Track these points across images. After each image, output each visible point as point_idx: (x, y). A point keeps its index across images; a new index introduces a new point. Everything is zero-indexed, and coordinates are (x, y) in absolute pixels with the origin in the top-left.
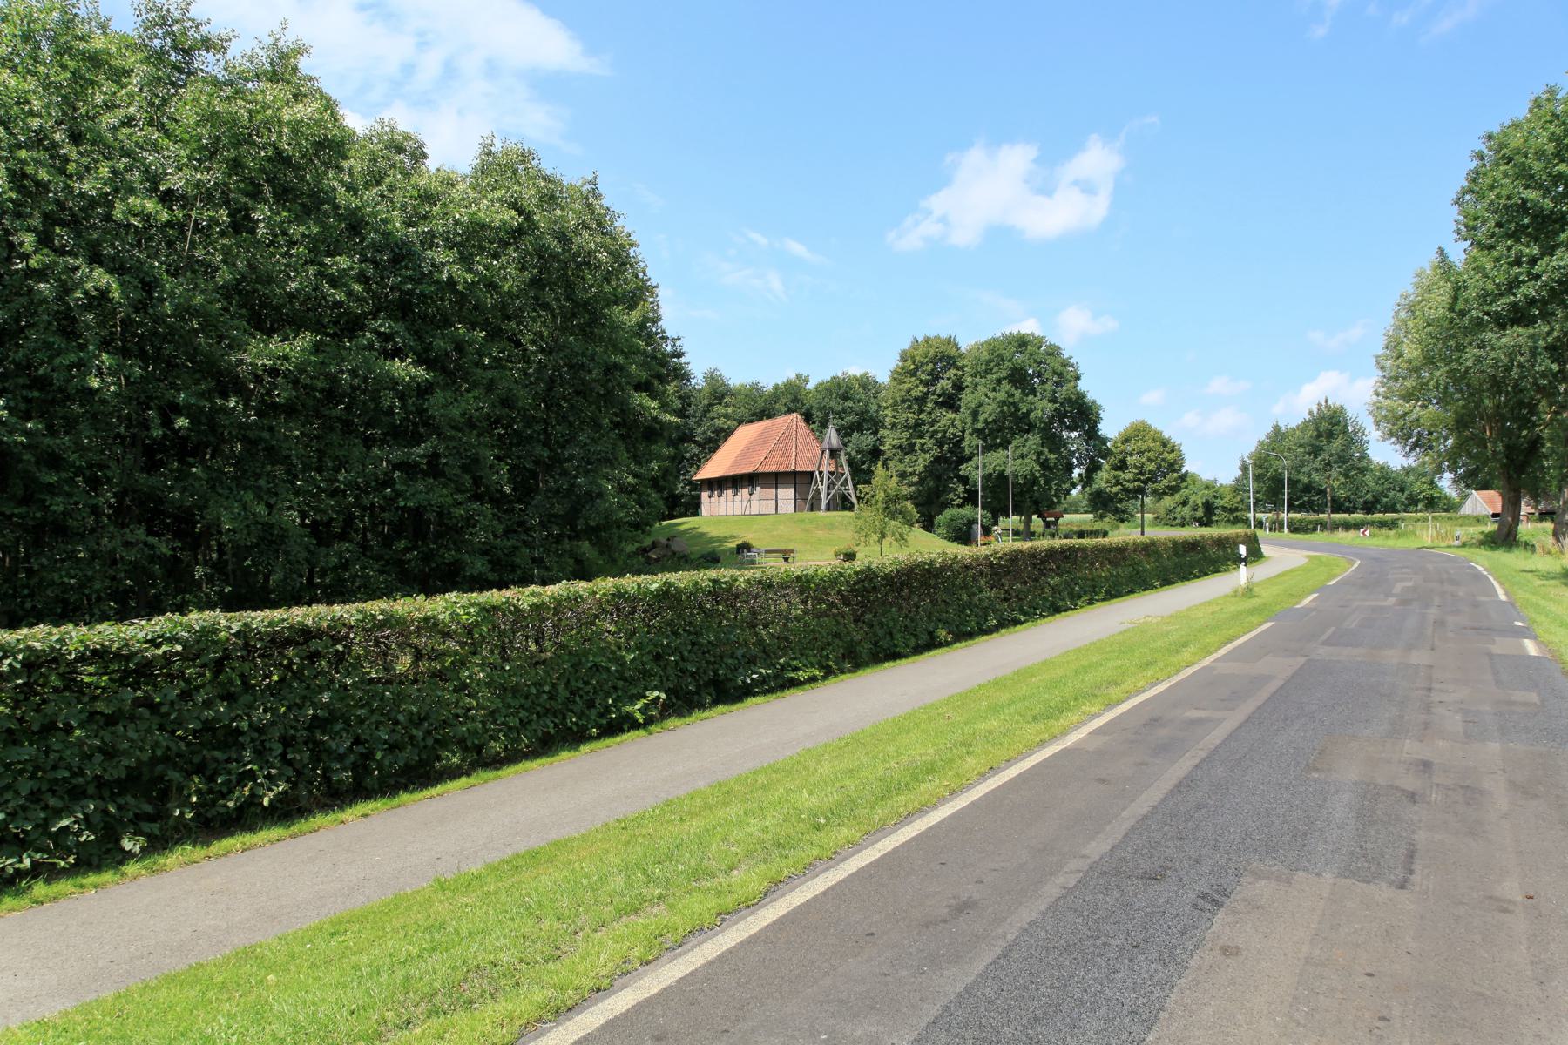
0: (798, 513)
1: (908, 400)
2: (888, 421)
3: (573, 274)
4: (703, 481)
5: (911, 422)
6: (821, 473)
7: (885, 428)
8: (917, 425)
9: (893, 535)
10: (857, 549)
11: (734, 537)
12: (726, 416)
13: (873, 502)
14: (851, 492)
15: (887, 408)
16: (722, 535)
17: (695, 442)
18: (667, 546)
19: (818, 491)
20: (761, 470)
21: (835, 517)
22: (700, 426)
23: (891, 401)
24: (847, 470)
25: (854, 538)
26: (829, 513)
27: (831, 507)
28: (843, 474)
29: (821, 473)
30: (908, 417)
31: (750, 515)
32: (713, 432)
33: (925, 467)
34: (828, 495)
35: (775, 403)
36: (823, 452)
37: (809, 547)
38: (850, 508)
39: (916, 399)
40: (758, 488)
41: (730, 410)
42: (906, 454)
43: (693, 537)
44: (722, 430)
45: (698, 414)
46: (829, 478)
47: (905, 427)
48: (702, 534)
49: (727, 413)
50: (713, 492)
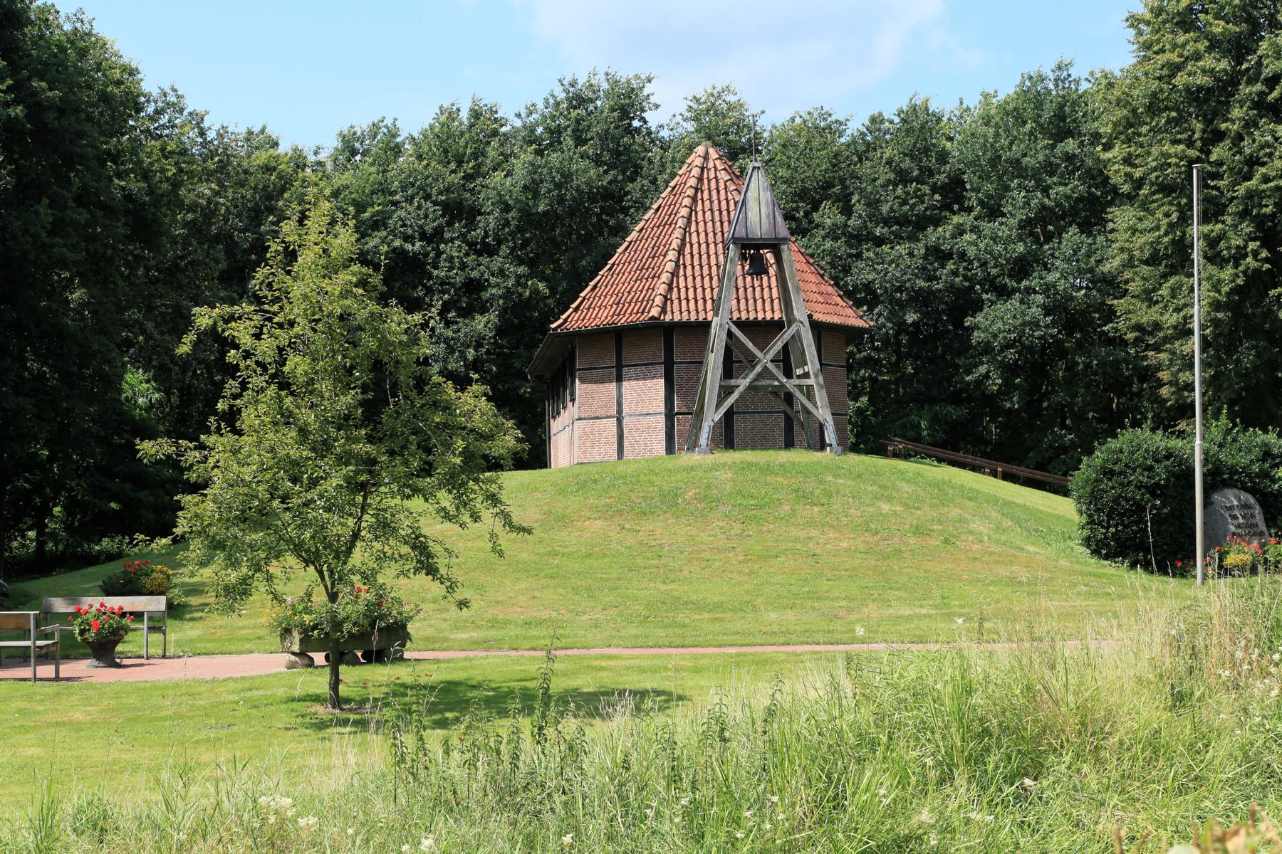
21: (715, 467)
30: (1165, 155)
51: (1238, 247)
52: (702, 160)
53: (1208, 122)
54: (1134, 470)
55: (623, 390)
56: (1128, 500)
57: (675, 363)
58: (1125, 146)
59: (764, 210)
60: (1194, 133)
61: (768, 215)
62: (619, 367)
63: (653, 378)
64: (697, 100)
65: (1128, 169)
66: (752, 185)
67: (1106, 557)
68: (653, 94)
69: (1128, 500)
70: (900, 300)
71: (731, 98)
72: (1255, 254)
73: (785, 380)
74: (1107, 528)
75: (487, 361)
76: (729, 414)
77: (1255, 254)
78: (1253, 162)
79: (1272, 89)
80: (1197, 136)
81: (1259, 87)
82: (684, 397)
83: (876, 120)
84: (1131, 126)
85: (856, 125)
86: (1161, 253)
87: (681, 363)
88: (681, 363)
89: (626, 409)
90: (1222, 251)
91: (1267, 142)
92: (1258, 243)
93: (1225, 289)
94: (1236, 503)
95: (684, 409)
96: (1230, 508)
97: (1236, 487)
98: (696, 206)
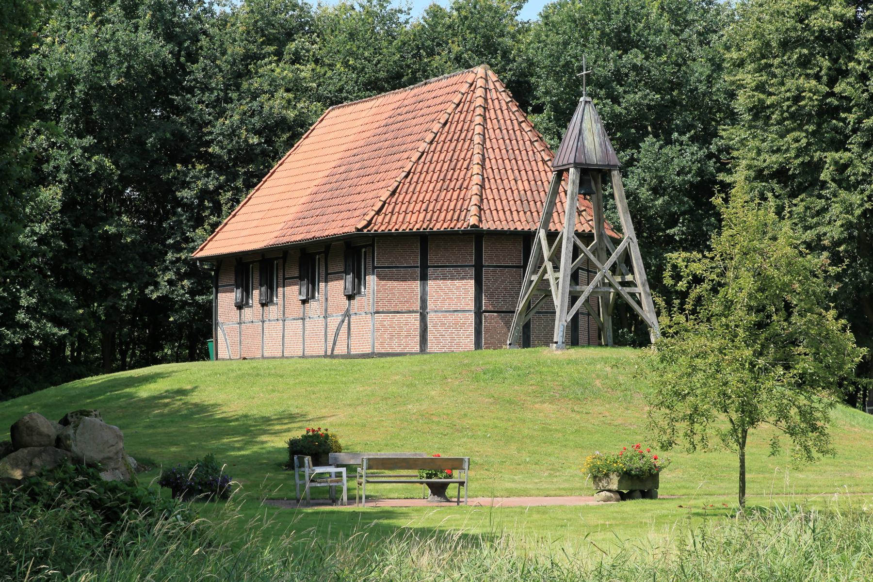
0: (484, 352)
1: (801, 42)
2: (741, 103)
3: (248, 97)
4: (221, 262)
5: (810, 103)
6: (552, 236)
7: (732, 117)
8: (826, 112)
9: (782, 414)
10: (663, 457)
11: (292, 418)
12: (296, 88)
13: (716, 307)
14: (641, 289)
15: (741, 64)
16: (255, 412)
17: (207, 158)
18: (59, 442)
19: (544, 289)
20: (381, 225)
21: (593, 362)
22: (221, 114)
23: (752, 45)
24: (629, 231)
25: (653, 425)
26: (575, 353)
27: (583, 336)
28: (616, 242)
29: (552, 236)
30: (799, 89)
31: (348, 356)
32: (258, 133)
33: (848, 226)
34: (573, 299)
35: (431, 53)
36: (560, 174)
37: (512, 450)
38: (642, 339)
39: (823, 37)
40: (372, 280)
41: (306, 71)
42: (793, 195)
43: (175, 417)
44: (282, 124)
45: (217, 81)
46: (576, 251)
47: (793, 117)
48: (201, 408)
49: (297, 80)
50: (247, 292)
51: (864, 174)
52: (484, 81)
53: (835, 61)
55: (429, 289)
58: (757, 74)
59: (597, 139)
60: (821, 69)
61: (601, 145)
62: (424, 267)
63: (462, 279)
65: (762, 96)
66: (585, 117)
73: (620, 288)
75: (53, 236)
76: (575, 320)
80: (823, 72)
83: (435, 13)
86: (790, 173)
87: (488, 266)
88: (488, 266)
89: (430, 305)
90: (849, 176)
93: (858, 212)
95: (491, 308)
98: (487, 124)
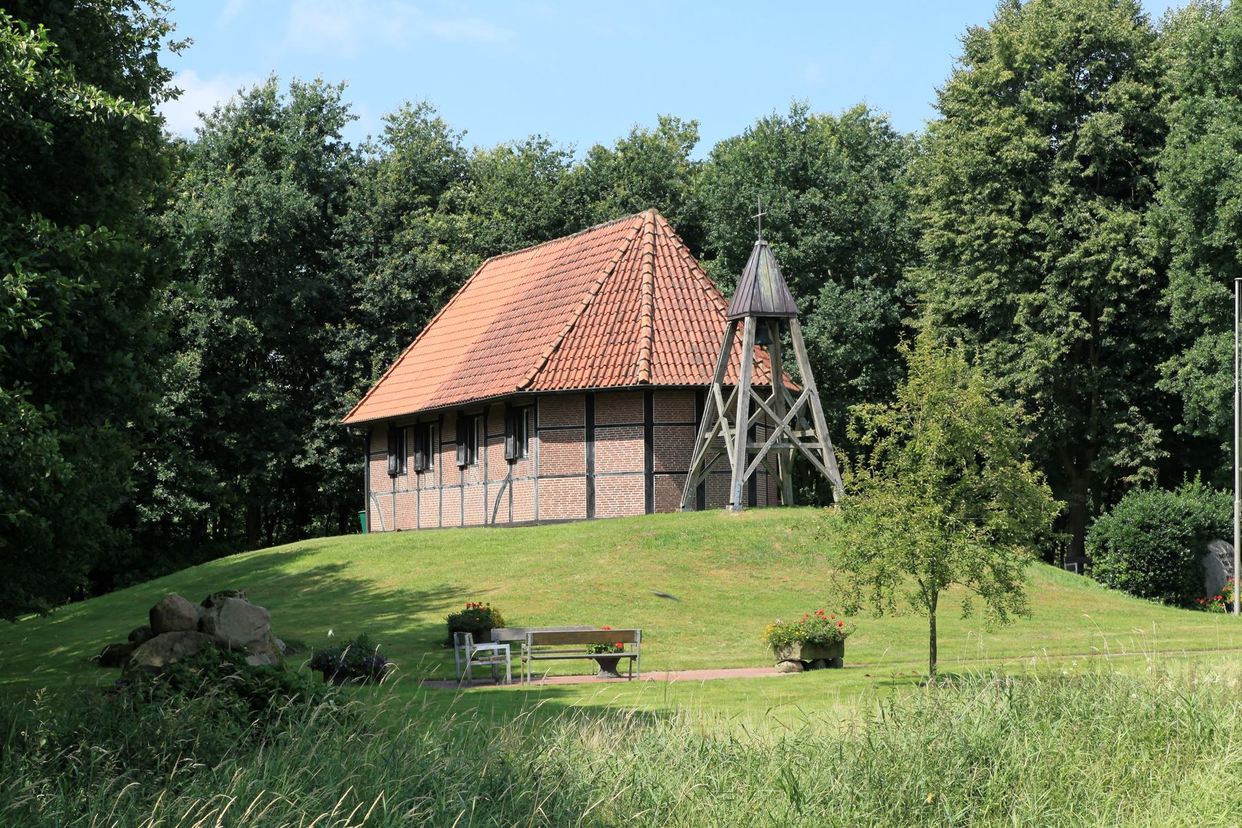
21: (772, 523)
30: (992, 227)
54: (1167, 524)
55: (595, 450)
56: (1165, 549)
57: (653, 425)
59: (773, 286)
60: (1014, 204)
61: (778, 291)
64: (393, 119)
65: (952, 235)
66: (761, 262)
67: (1146, 596)
68: (350, 105)
69: (1165, 549)
70: (400, 320)
71: (431, 118)
72: (1077, 325)
74: (1147, 573)
75: (191, 405)
76: (752, 479)
77: (1077, 325)
78: (1073, 236)
79: (1086, 167)
81: (1075, 163)
82: (662, 457)
84: (952, 193)
85: (580, 159)
87: (659, 424)
88: (659, 424)
89: (597, 468)
90: (1044, 319)
91: (1085, 218)
92: (1079, 314)
93: (1054, 357)
94: (1225, 552)
95: (662, 469)
96: (1222, 556)
97: (1223, 539)
